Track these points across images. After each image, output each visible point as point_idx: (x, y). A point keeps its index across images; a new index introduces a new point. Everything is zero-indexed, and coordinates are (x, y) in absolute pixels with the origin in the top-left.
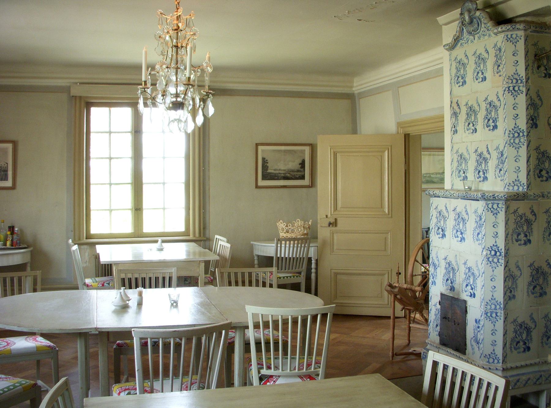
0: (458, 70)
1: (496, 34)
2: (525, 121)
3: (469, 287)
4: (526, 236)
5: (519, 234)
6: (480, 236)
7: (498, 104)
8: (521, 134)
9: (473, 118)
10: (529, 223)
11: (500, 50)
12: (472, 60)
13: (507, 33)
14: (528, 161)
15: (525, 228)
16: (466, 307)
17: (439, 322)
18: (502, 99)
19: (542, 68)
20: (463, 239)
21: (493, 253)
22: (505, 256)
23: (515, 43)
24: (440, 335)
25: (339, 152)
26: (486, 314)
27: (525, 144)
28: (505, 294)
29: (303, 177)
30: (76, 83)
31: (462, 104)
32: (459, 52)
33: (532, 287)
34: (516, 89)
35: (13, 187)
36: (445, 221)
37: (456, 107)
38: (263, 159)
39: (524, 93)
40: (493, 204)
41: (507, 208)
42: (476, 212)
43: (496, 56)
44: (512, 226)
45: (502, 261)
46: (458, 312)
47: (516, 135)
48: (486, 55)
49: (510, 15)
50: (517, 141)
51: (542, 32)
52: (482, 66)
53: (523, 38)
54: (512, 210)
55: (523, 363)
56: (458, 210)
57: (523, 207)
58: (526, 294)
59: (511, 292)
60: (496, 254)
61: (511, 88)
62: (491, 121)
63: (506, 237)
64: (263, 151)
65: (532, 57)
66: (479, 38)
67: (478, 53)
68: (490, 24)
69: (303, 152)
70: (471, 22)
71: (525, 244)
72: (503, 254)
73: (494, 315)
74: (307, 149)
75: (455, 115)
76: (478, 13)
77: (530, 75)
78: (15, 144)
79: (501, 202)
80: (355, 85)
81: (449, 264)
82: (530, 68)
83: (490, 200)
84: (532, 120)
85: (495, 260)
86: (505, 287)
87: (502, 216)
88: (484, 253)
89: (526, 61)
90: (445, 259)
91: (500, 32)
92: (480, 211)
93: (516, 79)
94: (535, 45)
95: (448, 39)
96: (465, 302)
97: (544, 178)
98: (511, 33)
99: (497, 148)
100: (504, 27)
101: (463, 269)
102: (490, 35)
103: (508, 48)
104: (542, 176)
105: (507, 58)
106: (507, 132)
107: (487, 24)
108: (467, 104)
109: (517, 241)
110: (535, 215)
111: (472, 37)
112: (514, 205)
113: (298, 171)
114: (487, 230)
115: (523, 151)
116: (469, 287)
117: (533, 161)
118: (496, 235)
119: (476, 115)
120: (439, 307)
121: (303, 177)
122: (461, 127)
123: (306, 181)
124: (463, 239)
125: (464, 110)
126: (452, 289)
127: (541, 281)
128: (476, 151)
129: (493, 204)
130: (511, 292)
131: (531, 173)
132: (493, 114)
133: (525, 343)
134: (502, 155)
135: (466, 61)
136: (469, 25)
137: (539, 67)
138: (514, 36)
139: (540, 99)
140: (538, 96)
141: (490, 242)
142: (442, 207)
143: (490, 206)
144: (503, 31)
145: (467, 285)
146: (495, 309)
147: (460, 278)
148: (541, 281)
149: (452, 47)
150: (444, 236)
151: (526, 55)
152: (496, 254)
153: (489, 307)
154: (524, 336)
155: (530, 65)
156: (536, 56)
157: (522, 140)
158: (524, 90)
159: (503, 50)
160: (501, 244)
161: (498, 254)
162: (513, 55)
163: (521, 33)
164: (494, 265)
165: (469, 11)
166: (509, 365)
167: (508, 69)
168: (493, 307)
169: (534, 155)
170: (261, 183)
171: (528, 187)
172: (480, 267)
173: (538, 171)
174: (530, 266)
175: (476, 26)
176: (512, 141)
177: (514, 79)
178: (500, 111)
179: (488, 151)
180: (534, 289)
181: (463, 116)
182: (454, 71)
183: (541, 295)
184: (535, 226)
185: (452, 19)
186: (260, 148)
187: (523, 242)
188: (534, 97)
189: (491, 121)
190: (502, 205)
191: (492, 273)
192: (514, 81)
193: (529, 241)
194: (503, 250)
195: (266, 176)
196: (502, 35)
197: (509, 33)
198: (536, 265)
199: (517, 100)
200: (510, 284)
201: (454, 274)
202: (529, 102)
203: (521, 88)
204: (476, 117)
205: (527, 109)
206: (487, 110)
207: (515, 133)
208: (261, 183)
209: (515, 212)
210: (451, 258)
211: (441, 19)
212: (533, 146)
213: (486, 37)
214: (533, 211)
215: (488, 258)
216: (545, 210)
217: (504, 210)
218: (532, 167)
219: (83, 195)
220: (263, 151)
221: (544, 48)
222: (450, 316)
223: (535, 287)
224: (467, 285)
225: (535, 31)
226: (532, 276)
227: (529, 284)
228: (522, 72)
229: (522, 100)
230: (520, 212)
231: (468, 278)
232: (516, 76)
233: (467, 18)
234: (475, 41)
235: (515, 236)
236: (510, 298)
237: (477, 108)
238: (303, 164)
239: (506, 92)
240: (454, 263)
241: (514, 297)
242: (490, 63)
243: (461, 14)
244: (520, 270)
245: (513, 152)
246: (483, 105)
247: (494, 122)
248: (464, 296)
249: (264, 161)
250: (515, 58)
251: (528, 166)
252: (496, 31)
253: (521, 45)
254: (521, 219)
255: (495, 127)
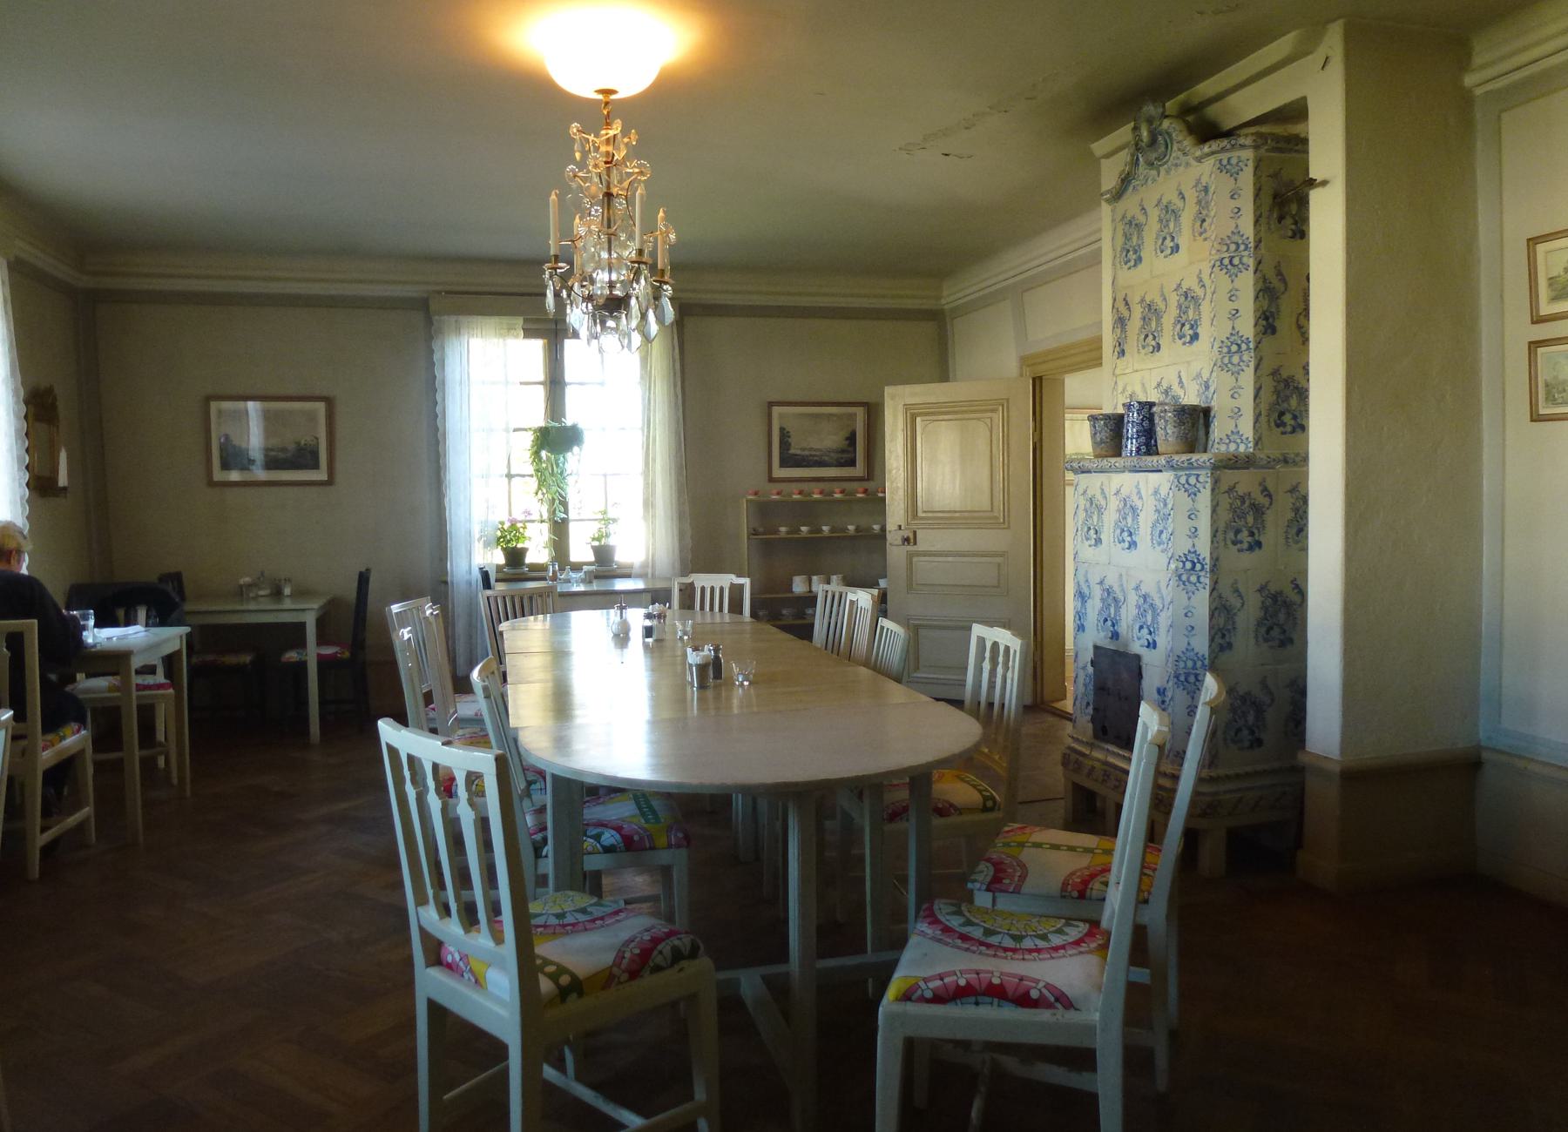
0: (1127, 237)
1: (1199, 160)
2: (1252, 322)
3: (1145, 631)
4: (1252, 534)
5: (1238, 532)
6: (1164, 536)
7: (1199, 292)
8: (1244, 347)
9: (1154, 324)
10: (1258, 510)
11: (1206, 189)
12: (1154, 214)
13: (1219, 156)
14: (1256, 397)
15: (1250, 519)
16: (1140, 668)
17: (1091, 698)
18: (1207, 281)
19: (1288, 221)
20: (1133, 545)
21: (1189, 565)
22: (1212, 571)
23: (1235, 175)
24: (1093, 720)
25: (920, 414)
26: (1177, 677)
27: (1252, 365)
28: (1212, 640)
29: (852, 463)
30: (439, 292)
31: (1135, 300)
32: (1130, 204)
33: (1263, 630)
34: (1236, 261)
35: (330, 482)
36: (1100, 514)
37: (1123, 309)
38: (782, 429)
39: (1251, 269)
40: (1188, 476)
41: (1216, 482)
42: (1156, 492)
43: (1199, 202)
44: (1225, 516)
45: (1206, 580)
46: (1125, 675)
47: (1234, 348)
48: (1180, 204)
49: (1228, 124)
50: (1236, 359)
51: (1290, 150)
52: (1172, 225)
53: (1251, 164)
54: (1224, 487)
55: (1249, 769)
56: (1124, 492)
57: (1246, 482)
58: (1252, 641)
59: (1223, 636)
60: (1193, 568)
61: (1226, 262)
62: (1187, 326)
63: (1214, 536)
64: (781, 416)
65: (1267, 200)
66: (1168, 172)
67: (1164, 201)
68: (1188, 142)
69: (852, 416)
70: (1153, 142)
71: (1251, 548)
72: (1207, 567)
73: (1192, 679)
74: (860, 412)
75: (1121, 322)
76: (1166, 123)
77: (1262, 234)
78: (329, 401)
79: (1202, 472)
80: (945, 293)
81: (1109, 591)
82: (1263, 220)
83: (1182, 469)
84: (1266, 319)
85: (1194, 579)
86: (1211, 628)
87: (1205, 499)
88: (1173, 566)
89: (1257, 207)
90: (1101, 583)
91: (1208, 155)
92: (1164, 492)
93: (1238, 245)
94: (1275, 176)
95: (1109, 181)
96: (1138, 657)
97: (1289, 429)
98: (1228, 155)
99: (1199, 375)
100: (1215, 145)
101: (1133, 598)
102: (1188, 164)
103: (1221, 186)
104: (1284, 424)
105: (1220, 207)
106: (1216, 345)
107: (1183, 141)
108: (1143, 300)
109: (1235, 543)
110: (1270, 496)
111: (1154, 172)
112: (1229, 477)
113: (843, 451)
114: (1179, 524)
115: (1248, 379)
116: (1145, 631)
117: (1267, 396)
118: (1194, 533)
119: (1159, 318)
120: (1090, 669)
121: (852, 463)
122: (1131, 345)
123: (859, 470)
124: (1133, 545)
125: (1137, 311)
126: (1115, 636)
127: (1282, 617)
128: (1159, 385)
129: (1188, 476)
130: (1223, 636)
131: (1263, 419)
132: (1191, 312)
133: (1252, 732)
134: (1207, 387)
135: (1142, 219)
136: (1151, 150)
137: (1281, 219)
138: (1234, 161)
139: (1283, 280)
140: (1279, 274)
141: (1183, 546)
142: (1094, 491)
143: (1183, 480)
144: (1213, 153)
145: (1141, 628)
146: (1194, 667)
147: (1128, 615)
148: (1282, 617)
149: (1118, 195)
150: (1098, 541)
151: (1257, 196)
152: (1193, 568)
153: (1182, 665)
154: (1251, 718)
155: (1265, 214)
156: (1275, 197)
157: (1245, 358)
158: (1251, 262)
159: (1211, 190)
160: (1204, 550)
161: (1198, 567)
162: (1232, 197)
163: (1248, 154)
164: (1190, 588)
165: (1150, 121)
166: (1221, 772)
167: (1221, 225)
168: (1190, 664)
169: (1268, 384)
170: (778, 472)
171: (1256, 444)
172: (1164, 591)
173: (1276, 415)
174: (1261, 590)
175: (1163, 149)
176: (1226, 360)
177: (1232, 242)
178: (1206, 307)
179: (1181, 382)
180: (1268, 632)
181: (1135, 324)
182: (1120, 240)
183: (1283, 644)
184: (1269, 517)
185: (1118, 143)
186: (776, 410)
187: (1245, 546)
188: (1271, 274)
189: (1187, 326)
190: (1205, 477)
191: (1185, 602)
192: (1233, 247)
193: (1259, 544)
194: (1208, 561)
195: (787, 461)
196: (1211, 161)
197: (1224, 157)
198: (1273, 588)
199: (1238, 283)
200: (1222, 621)
201: (1118, 608)
202: (1260, 285)
203: (1245, 260)
204: (1140, 236)
205: (1257, 297)
206: (1180, 306)
207: (1231, 346)
208: (778, 472)
209: (1231, 489)
210: (1111, 580)
211: (1100, 147)
212: (1267, 367)
213: (1181, 169)
214: (1265, 489)
215: (1180, 576)
216: (1289, 487)
217: (1208, 486)
218: (1264, 407)
219: (804, 880)
220: (781, 416)
221: (1292, 181)
222: (1110, 684)
223: (1270, 629)
224: (1141, 628)
225: (1274, 150)
226: (1265, 608)
227: (1259, 624)
228: (1247, 228)
229: (1247, 282)
230: (1241, 490)
231: (1142, 614)
232: (1236, 238)
233: (1145, 134)
234: (1161, 179)
235: (1231, 535)
236: (1222, 648)
237: (1162, 306)
238: (852, 439)
239: (1216, 269)
240: (1116, 588)
241: (1230, 646)
242: (1187, 217)
243: (1135, 129)
244: (1240, 596)
245: (1228, 379)
246: (1174, 299)
247: (1192, 327)
248: (1137, 648)
249: (784, 435)
250: (1233, 204)
251: (1256, 405)
252: (1198, 153)
253: (1247, 178)
254: (1243, 502)
255: (1195, 337)
